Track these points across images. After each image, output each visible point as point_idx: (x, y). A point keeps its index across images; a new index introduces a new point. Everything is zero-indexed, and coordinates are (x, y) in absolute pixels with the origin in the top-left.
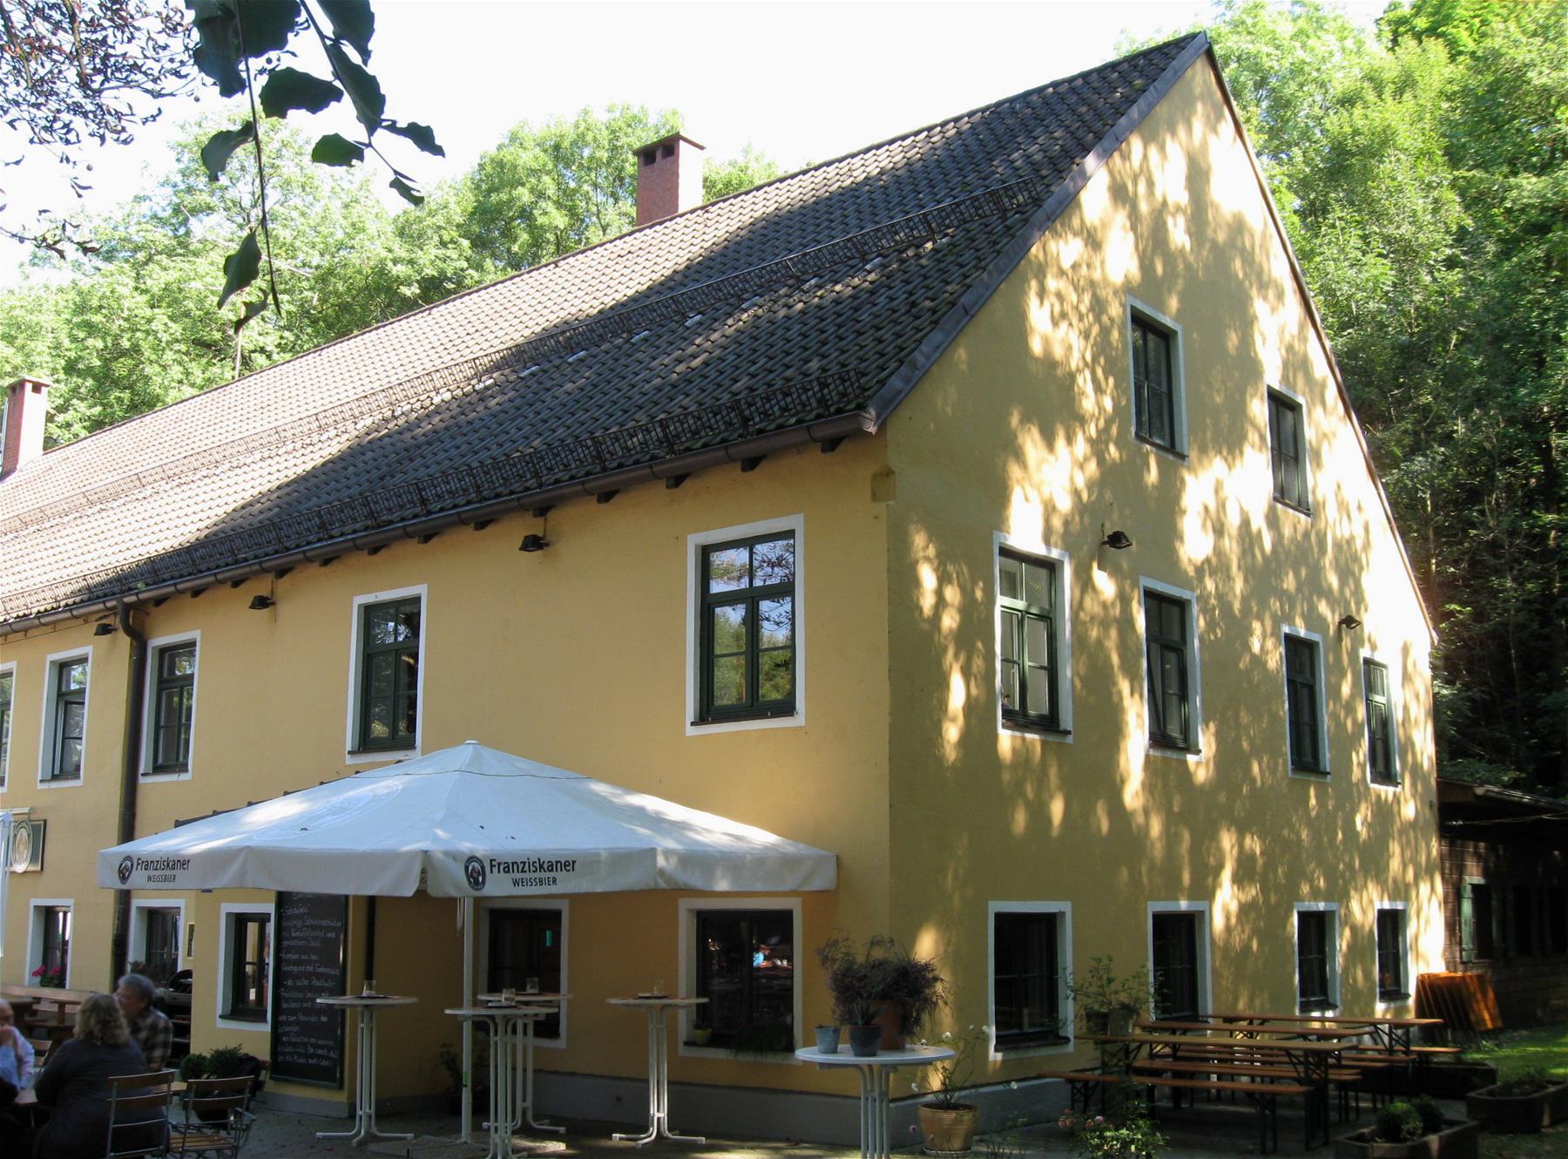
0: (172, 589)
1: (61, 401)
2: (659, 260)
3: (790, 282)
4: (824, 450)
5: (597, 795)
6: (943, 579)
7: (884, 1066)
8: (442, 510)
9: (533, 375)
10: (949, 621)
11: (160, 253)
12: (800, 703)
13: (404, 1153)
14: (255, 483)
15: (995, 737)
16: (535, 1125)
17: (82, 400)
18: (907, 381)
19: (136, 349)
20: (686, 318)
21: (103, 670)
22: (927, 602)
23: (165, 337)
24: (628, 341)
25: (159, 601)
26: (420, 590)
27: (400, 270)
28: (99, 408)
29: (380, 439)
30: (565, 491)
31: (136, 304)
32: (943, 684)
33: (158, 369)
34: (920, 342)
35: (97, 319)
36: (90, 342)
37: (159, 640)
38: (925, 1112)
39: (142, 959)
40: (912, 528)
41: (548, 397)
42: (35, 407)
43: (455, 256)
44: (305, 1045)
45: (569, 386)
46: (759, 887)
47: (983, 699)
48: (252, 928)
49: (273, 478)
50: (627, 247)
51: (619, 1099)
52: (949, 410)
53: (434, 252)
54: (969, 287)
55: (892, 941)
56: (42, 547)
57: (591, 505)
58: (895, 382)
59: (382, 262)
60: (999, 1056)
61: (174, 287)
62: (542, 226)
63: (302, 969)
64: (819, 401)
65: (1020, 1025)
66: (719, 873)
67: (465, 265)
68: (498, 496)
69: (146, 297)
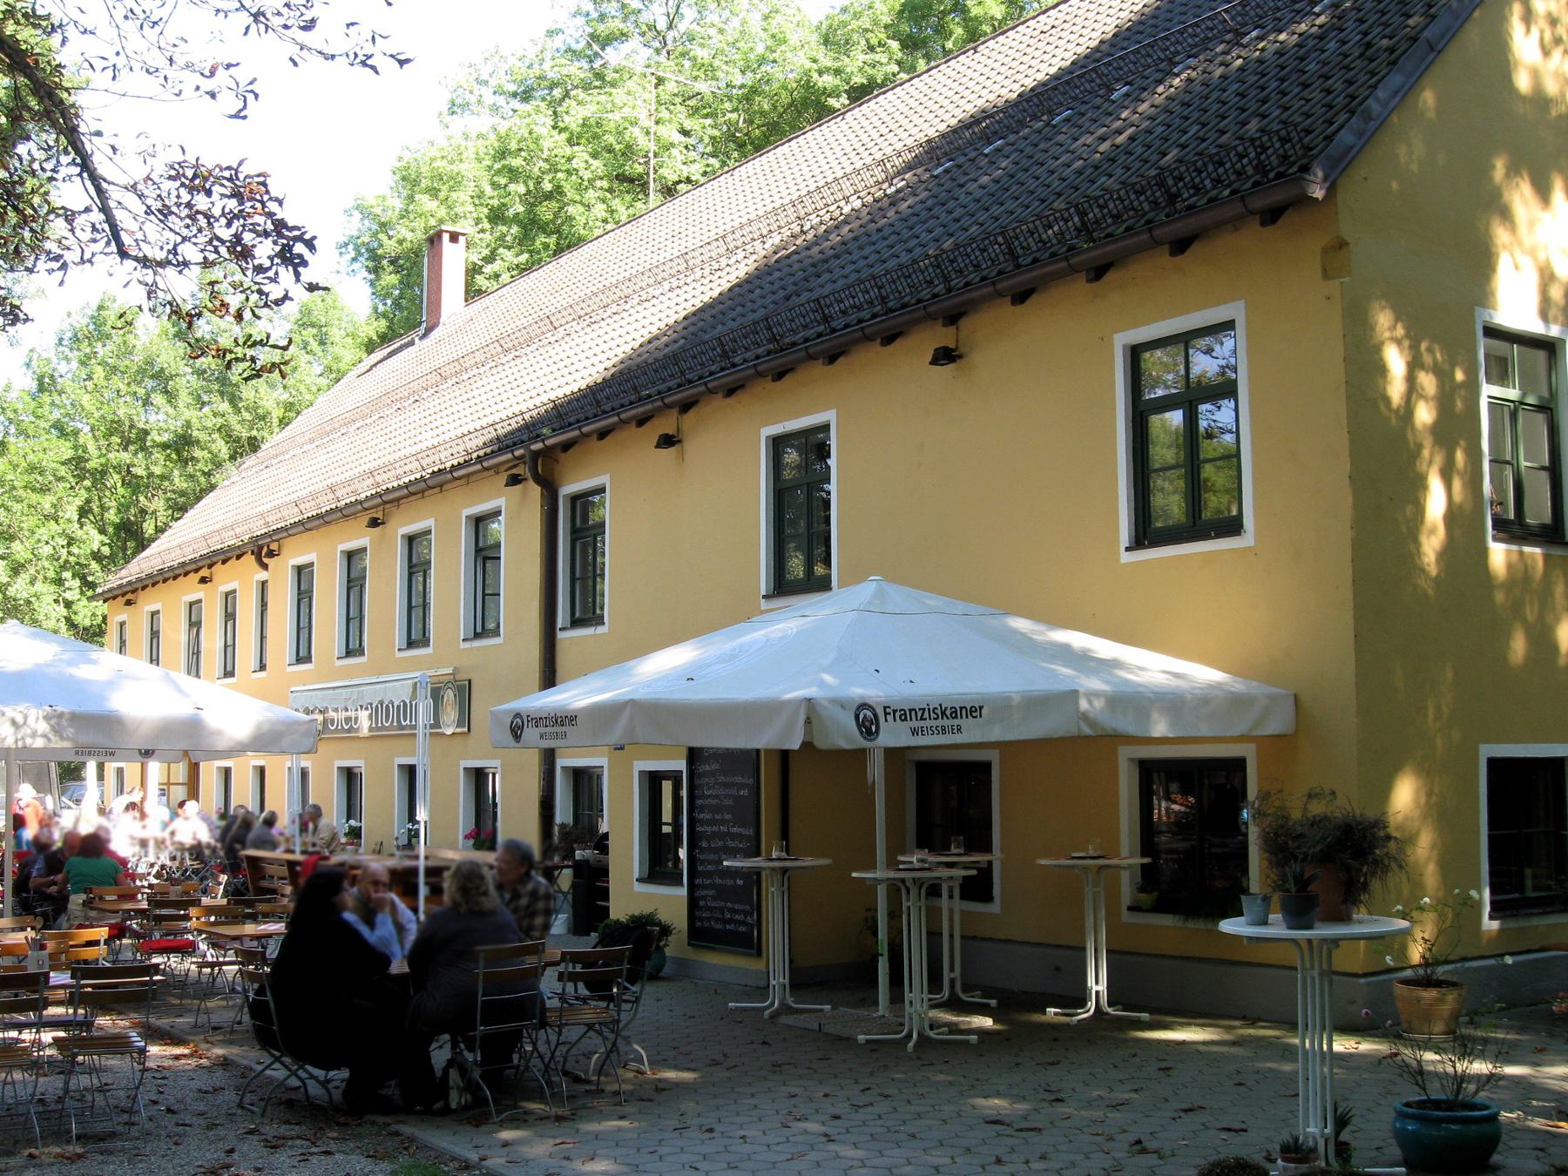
0: (577, 433)
1: (486, 252)
2: (1084, 32)
3: (1228, 37)
4: (1263, 224)
5: (1016, 632)
6: (1414, 366)
7: (1324, 940)
8: (846, 326)
9: (946, 171)
10: (1424, 414)
11: (577, 87)
12: (1248, 521)
13: (816, 1027)
14: (662, 315)
15: (1484, 553)
16: (964, 997)
17: (509, 248)
18: (1361, 134)
19: (558, 190)
20: (1111, 90)
21: (517, 521)
22: (1396, 390)
23: (587, 175)
24: (1048, 124)
25: (567, 446)
26: (829, 416)
27: (828, 81)
28: (526, 256)
29: (788, 257)
30: (976, 294)
31: (553, 143)
32: (1418, 485)
33: (581, 209)
34: (1375, 87)
35: (517, 162)
36: (512, 187)
37: (569, 488)
38: (1400, 989)
39: (570, 820)
40: (1375, 306)
41: (961, 194)
42: (454, 260)
43: (884, 60)
44: (722, 910)
45: (985, 179)
46: (1204, 730)
47: (1468, 507)
48: (667, 787)
49: (680, 308)
50: (1051, 22)
51: (1057, 969)
52: (1414, 167)
53: (862, 57)
54: (1434, 17)
55: (1333, 793)
56: (459, 400)
57: (1005, 309)
58: (1346, 137)
59: (807, 73)
60: (1495, 925)
61: (592, 121)
62: (976, 18)
63: (715, 829)
64: (1256, 168)
65: (1520, 888)
66: (1155, 715)
67: (896, 68)
68: (904, 306)
69: (565, 136)
